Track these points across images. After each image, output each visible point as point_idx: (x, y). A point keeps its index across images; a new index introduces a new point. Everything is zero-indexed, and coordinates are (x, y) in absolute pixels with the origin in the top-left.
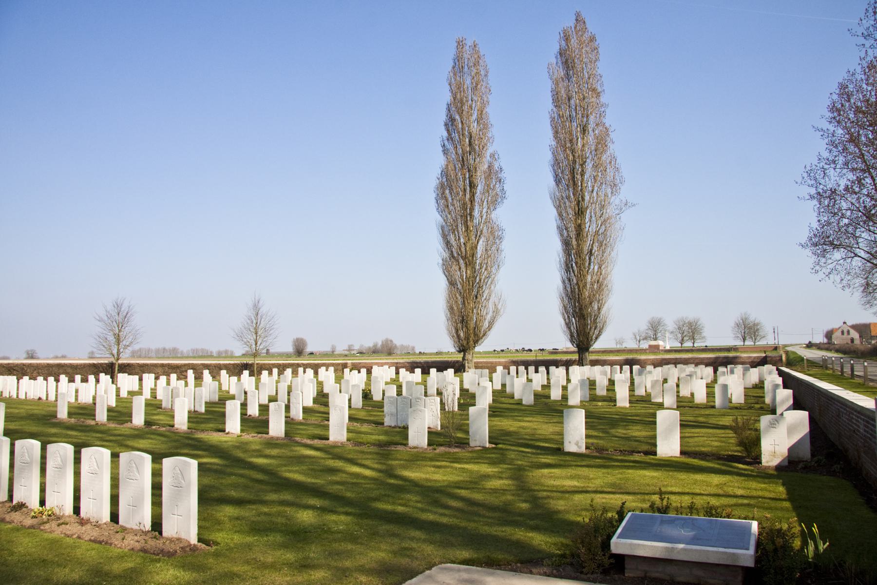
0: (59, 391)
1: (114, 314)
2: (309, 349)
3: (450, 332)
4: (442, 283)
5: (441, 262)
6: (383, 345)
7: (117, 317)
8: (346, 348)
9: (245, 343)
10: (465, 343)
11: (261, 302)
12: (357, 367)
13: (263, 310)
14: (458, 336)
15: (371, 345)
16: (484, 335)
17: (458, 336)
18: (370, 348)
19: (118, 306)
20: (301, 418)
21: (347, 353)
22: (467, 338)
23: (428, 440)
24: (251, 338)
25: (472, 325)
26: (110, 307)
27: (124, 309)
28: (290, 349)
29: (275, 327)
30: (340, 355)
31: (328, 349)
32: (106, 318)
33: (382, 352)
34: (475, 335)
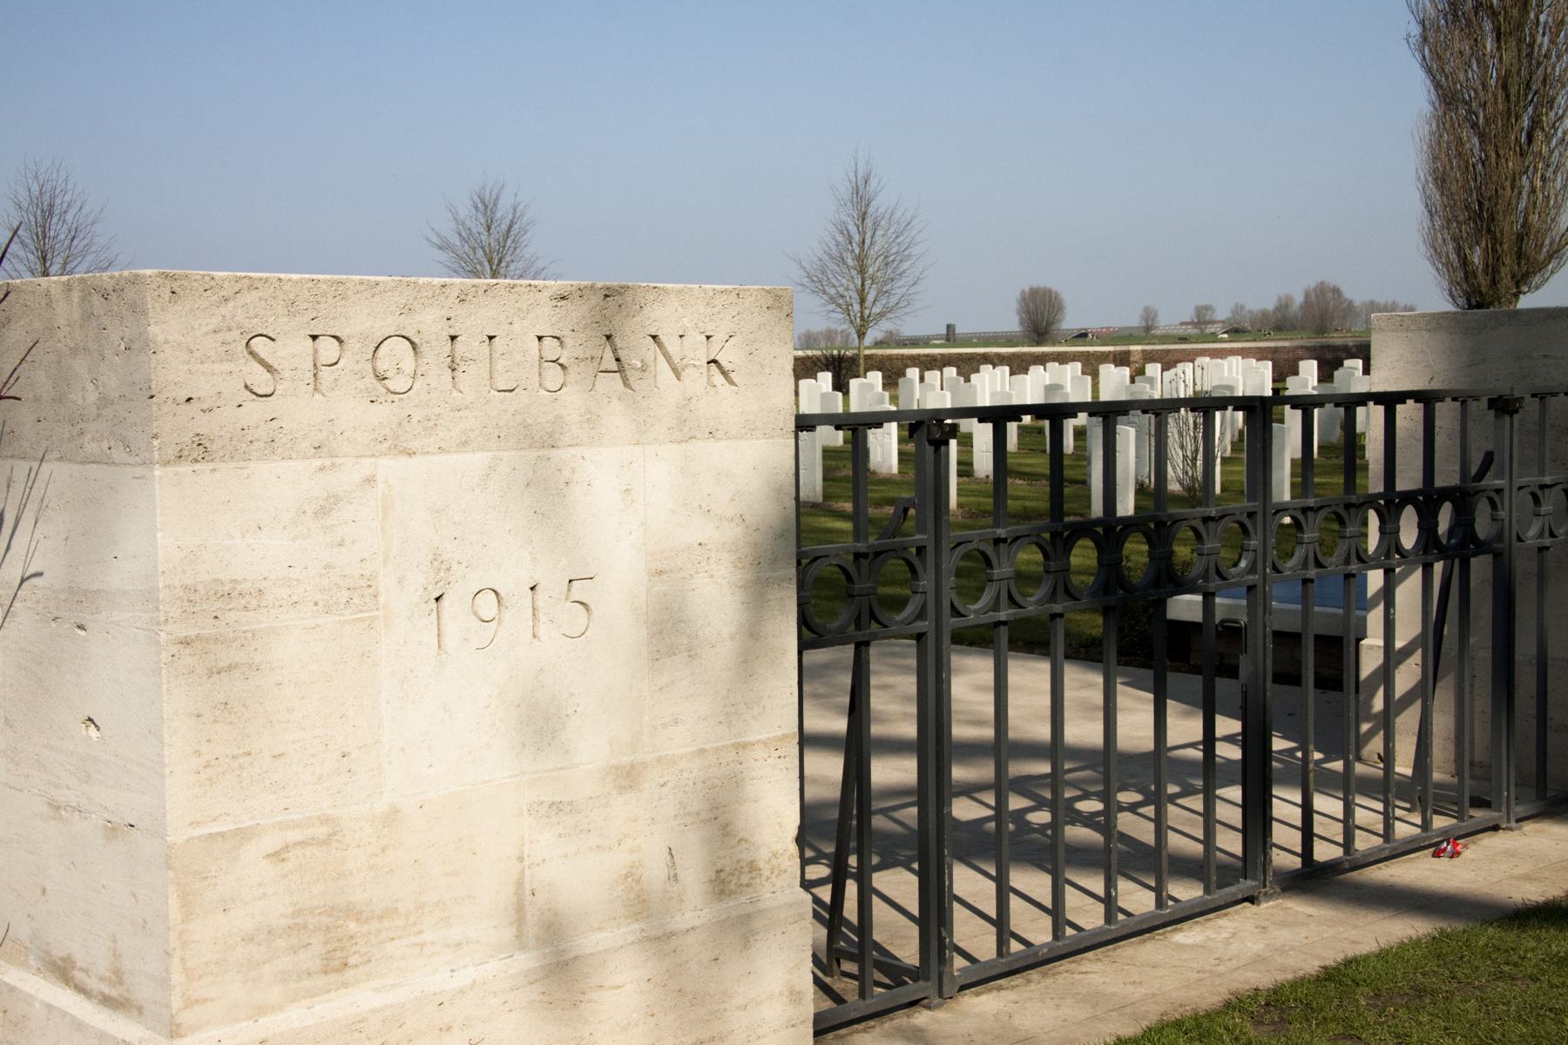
0: (806, 772)
1: (477, 227)
2: (1071, 321)
3: (1436, 252)
4: (1413, 98)
5: (1416, 30)
6: (1307, 303)
7: (484, 237)
8: (1188, 314)
9: (832, 300)
10: (1483, 281)
11: (873, 183)
12: (1121, 360)
13: (880, 205)
14: (1465, 261)
15: (1270, 305)
16: (1550, 257)
17: (1465, 261)
18: (1264, 314)
19: (486, 207)
20: (895, 470)
21: (1191, 331)
22: (1493, 270)
23: (1136, 501)
24: (846, 284)
25: (1509, 226)
26: (465, 210)
27: (503, 212)
28: (1011, 323)
29: (915, 251)
30: (1164, 339)
31: (1134, 321)
32: (456, 241)
33: (1303, 328)
34: (1520, 255)
